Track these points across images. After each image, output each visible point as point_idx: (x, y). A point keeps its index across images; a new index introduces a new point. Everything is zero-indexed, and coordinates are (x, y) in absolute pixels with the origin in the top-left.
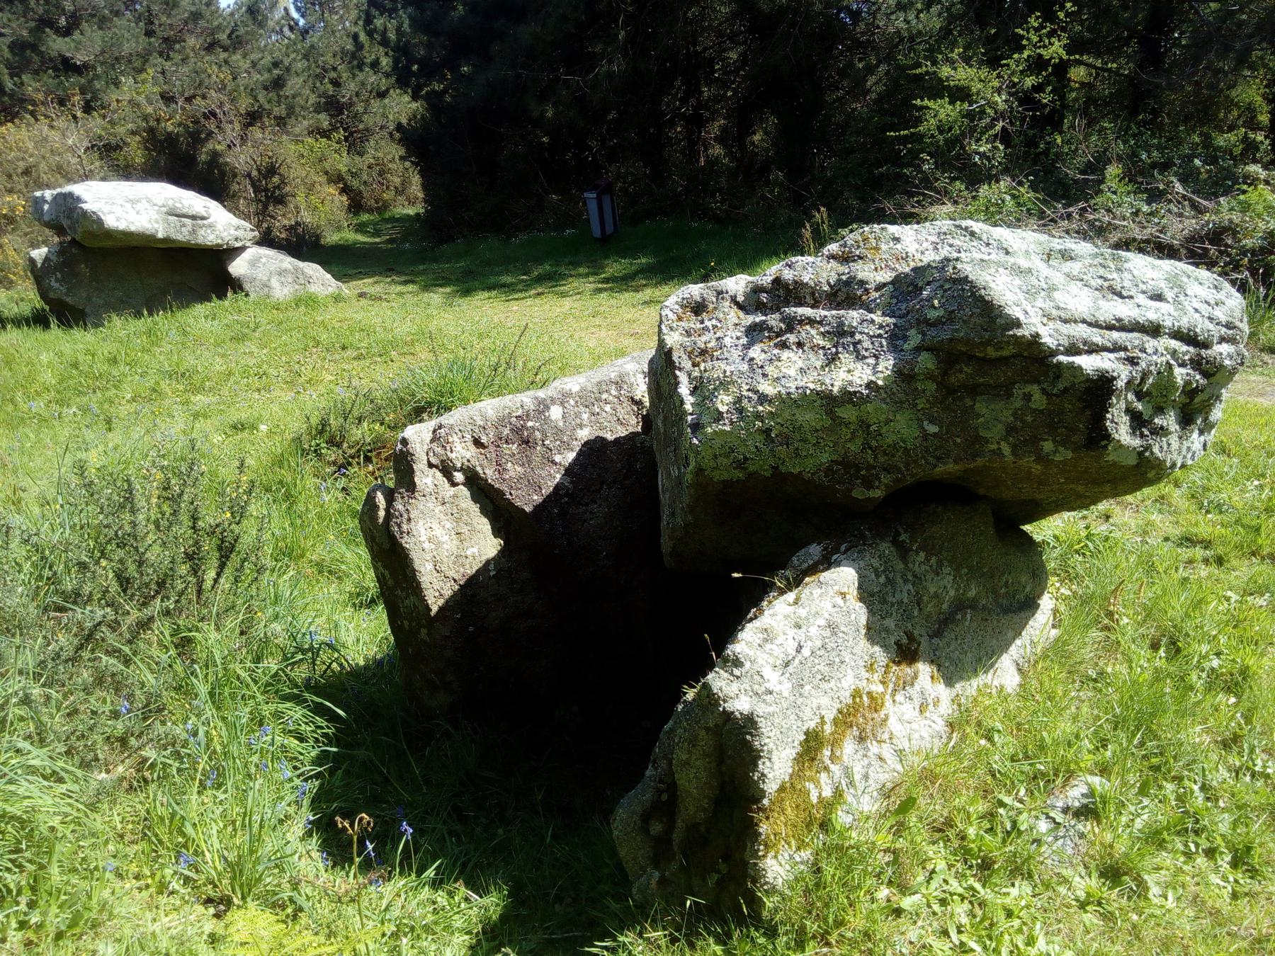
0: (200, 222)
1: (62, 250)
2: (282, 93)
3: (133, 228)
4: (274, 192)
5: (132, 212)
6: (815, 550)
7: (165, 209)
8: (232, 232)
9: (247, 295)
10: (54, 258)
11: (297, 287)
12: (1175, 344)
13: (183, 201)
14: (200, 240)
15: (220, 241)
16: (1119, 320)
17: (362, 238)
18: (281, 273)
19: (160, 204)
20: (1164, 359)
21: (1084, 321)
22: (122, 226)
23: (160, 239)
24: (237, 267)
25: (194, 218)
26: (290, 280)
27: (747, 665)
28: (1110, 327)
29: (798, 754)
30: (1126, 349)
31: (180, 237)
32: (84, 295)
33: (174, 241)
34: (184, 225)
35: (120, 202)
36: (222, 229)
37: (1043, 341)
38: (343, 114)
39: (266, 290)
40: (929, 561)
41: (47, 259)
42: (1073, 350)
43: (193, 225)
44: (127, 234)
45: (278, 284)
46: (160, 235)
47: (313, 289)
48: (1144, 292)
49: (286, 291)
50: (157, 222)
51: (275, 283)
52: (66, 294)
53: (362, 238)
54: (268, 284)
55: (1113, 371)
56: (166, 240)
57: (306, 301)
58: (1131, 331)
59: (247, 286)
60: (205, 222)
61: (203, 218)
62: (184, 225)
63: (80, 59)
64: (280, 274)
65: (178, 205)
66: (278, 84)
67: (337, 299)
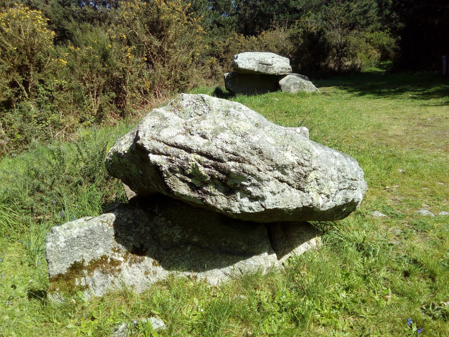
0: (269, 66)
1: (232, 74)
2: (365, 16)
3: (247, 68)
4: (344, 53)
5: (248, 62)
6: (216, 210)
7: (258, 62)
8: (280, 70)
9: (282, 91)
10: (230, 76)
11: (300, 89)
12: (198, 157)
13: (265, 59)
14: (268, 72)
15: (274, 73)
16: (176, 144)
17: (378, 70)
18: (295, 84)
19: (257, 60)
20: (194, 163)
21: (163, 142)
22: (243, 67)
23: (256, 72)
24: (282, 82)
25: (267, 65)
26: (298, 87)
27: (55, 233)
28: (173, 146)
29: (69, 267)
30: (170, 155)
31: (262, 71)
32: (236, 88)
33: (260, 72)
34: (264, 67)
35: (245, 59)
36: (276, 68)
37: (144, 147)
38: (393, 22)
39: (289, 89)
40: (167, 222)
41: (228, 76)
42: (156, 152)
43: (267, 67)
44: (245, 70)
45: (293, 88)
46: (256, 70)
47: (306, 90)
48: (199, 134)
49: (295, 90)
50: (255, 66)
51: (292, 87)
52: (231, 87)
53: (378, 70)
54: (290, 88)
55: (159, 163)
56: (258, 72)
57: (302, 95)
58: (181, 149)
59: (282, 88)
60: (271, 66)
61: (271, 65)
62: (264, 67)
63: (299, 7)
64: (294, 85)
65: (263, 61)
66: (365, 12)
67: (314, 94)
